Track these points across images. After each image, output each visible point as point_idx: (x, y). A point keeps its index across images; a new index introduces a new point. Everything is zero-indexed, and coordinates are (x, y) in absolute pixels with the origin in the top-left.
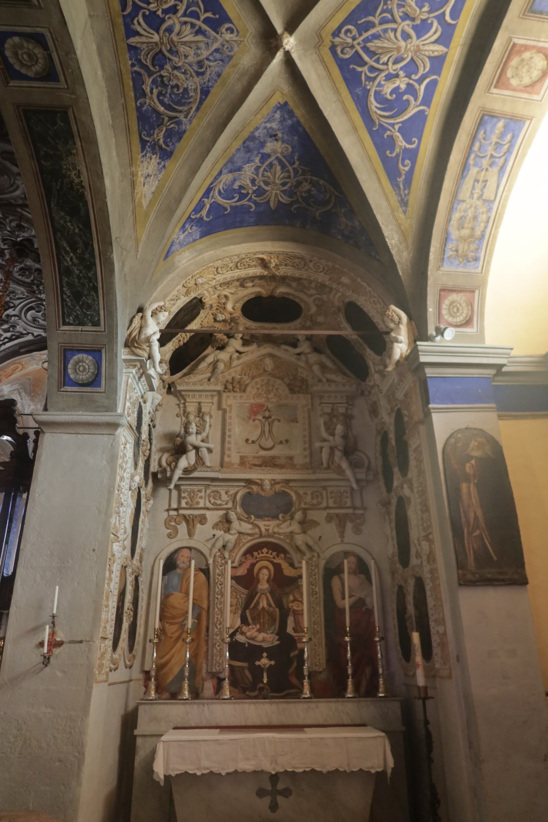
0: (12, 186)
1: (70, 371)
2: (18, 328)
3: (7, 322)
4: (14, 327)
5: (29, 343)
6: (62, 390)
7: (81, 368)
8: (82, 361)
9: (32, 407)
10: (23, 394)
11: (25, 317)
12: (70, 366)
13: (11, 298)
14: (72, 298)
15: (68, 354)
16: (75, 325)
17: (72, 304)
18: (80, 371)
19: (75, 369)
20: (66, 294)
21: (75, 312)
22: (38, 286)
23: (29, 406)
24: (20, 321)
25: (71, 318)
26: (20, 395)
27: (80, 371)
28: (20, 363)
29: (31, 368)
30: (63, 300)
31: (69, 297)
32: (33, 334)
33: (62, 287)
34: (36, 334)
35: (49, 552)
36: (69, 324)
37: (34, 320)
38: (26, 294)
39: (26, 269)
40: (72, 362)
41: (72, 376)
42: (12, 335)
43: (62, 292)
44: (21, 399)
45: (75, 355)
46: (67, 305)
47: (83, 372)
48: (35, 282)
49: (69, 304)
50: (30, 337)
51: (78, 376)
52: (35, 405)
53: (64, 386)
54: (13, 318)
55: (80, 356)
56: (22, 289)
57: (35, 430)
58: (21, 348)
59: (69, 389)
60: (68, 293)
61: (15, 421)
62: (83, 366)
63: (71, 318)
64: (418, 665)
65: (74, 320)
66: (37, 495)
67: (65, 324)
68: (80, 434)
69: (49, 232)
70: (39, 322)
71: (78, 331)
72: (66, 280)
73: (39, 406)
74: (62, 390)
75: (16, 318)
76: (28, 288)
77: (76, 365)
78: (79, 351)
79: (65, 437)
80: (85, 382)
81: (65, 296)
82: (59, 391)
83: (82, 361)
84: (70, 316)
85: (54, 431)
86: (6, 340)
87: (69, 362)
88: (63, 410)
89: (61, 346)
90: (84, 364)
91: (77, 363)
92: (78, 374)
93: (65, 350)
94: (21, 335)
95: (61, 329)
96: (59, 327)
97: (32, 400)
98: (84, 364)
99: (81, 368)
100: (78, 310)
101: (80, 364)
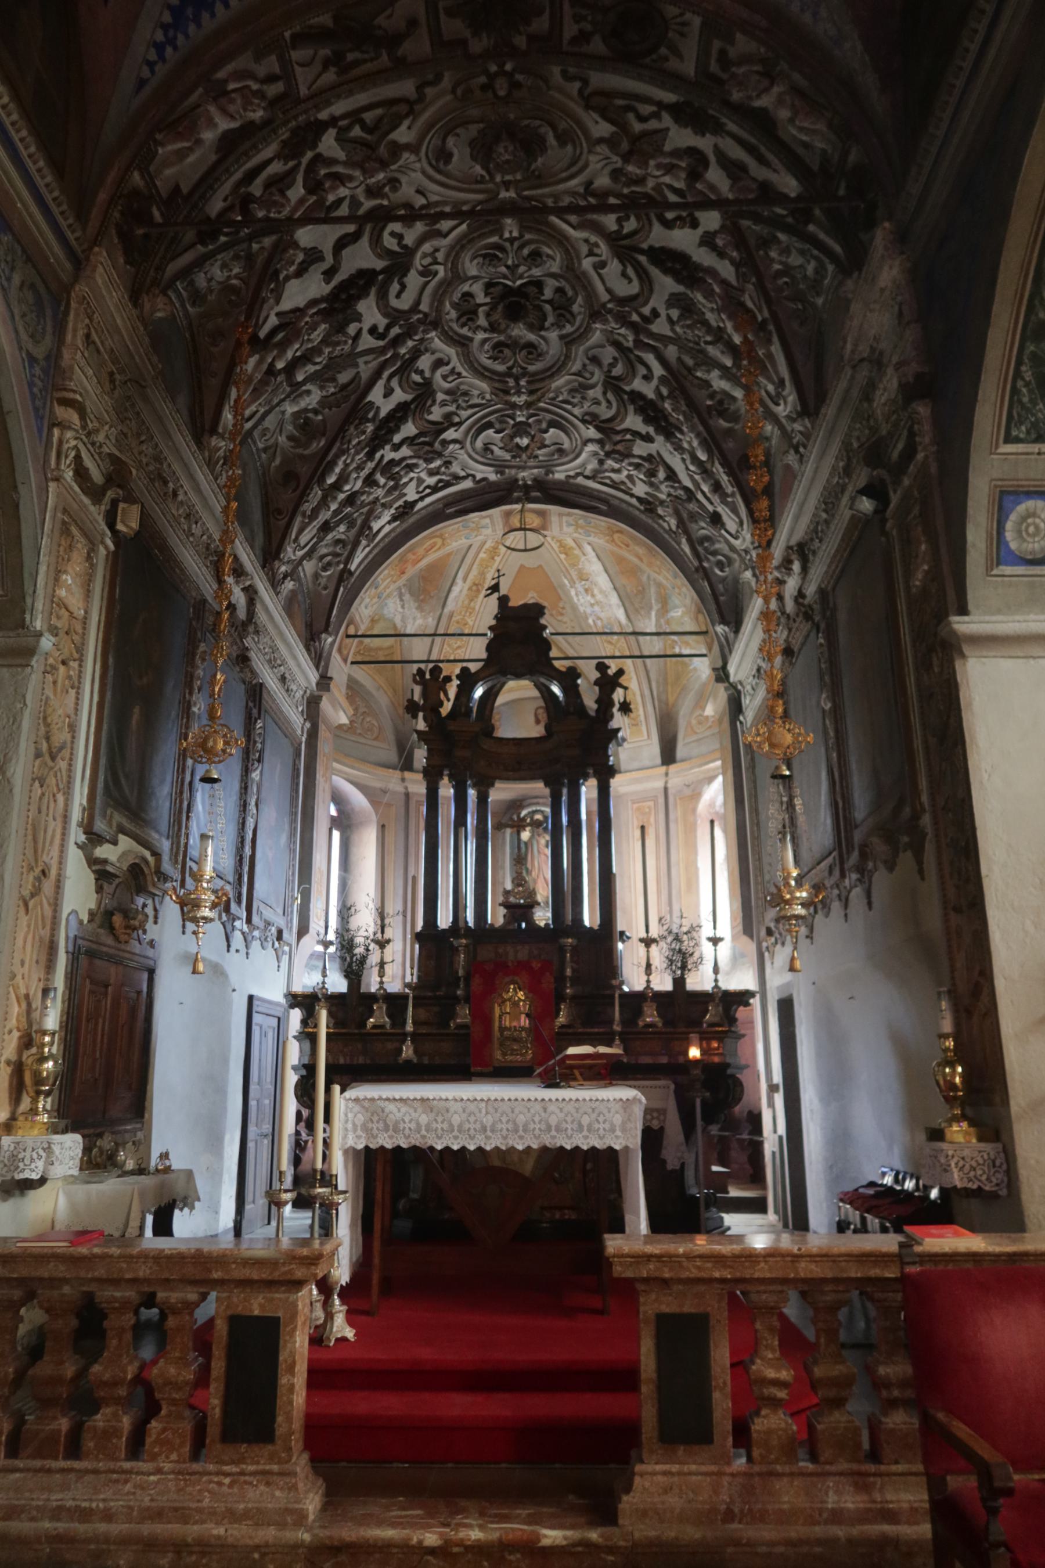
0: (573, 164)
1: (1009, 535)
2: (456, 468)
3: (440, 455)
4: (447, 464)
5: (464, 495)
6: (995, 572)
7: (1031, 529)
8: (1034, 515)
9: (419, 621)
10: (407, 597)
11: (473, 443)
12: (1009, 525)
13: (458, 407)
14: (1034, 385)
15: (1008, 501)
16: (1029, 442)
17: (1031, 400)
18: (1028, 534)
19: (1019, 532)
20: (1023, 379)
21: (1033, 415)
22: (517, 379)
23: (414, 619)
24: (462, 452)
25: (1023, 428)
26: (401, 600)
27: (1028, 534)
28: (441, 536)
29: (454, 544)
30: (1015, 391)
31: (1027, 384)
32: (474, 476)
33: (1019, 363)
34: (479, 476)
35: (1037, 881)
36: (1018, 440)
37: (487, 448)
38: (488, 397)
39: (507, 346)
40: (1013, 517)
41: (1013, 546)
42: (440, 481)
43: (1018, 374)
44: (403, 607)
45: (1020, 503)
46: (1020, 402)
47: (1034, 535)
48: (514, 370)
49: (1025, 400)
50: (468, 484)
51: (1025, 545)
52: (425, 618)
53: (998, 564)
54: (451, 446)
55: (1030, 504)
56: (484, 386)
57: (596, 661)
58: (448, 505)
59: (1008, 570)
60: (1028, 376)
61: (547, 645)
62: (1034, 524)
63: (1023, 428)
64: (294, 1068)
65: (1028, 432)
66: (986, 776)
67: (1009, 439)
68: (1034, 658)
69: (1032, 252)
70: (492, 452)
71: (1032, 454)
72: (1032, 348)
73: (430, 620)
74: (995, 572)
75: (457, 446)
76: (497, 385)
77: (1021, 524)
78: (1029, 494)
79: (1007, 664)
80: (1039, 556)
81: (1020, 383)
82: (988, 575)
83: (1034, 515)
84: (1021, 423)
85: (985, 653)
86: (428, 491)
87: (1007, 517)
88: (999, 612)
89: (996, 486)
90: (1037, 521)
91: (1024, 519)
92: (1024, 540)
93: (1002, 493)
94: (457, 478)
95: (1001, 450)
96: (997, 447)
97: (420, 608)
98: (1037, 521)
99: (1031, 529)
100: (1040, 411)
101: (1030, 521)
